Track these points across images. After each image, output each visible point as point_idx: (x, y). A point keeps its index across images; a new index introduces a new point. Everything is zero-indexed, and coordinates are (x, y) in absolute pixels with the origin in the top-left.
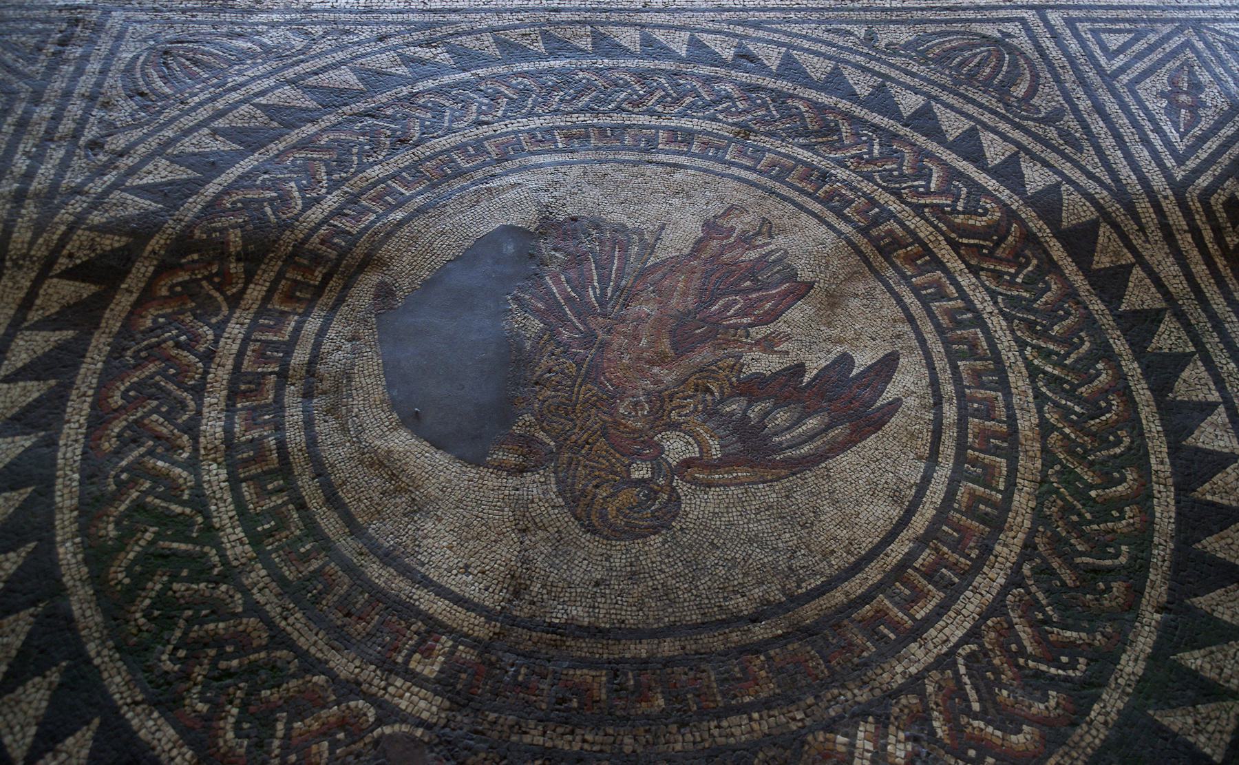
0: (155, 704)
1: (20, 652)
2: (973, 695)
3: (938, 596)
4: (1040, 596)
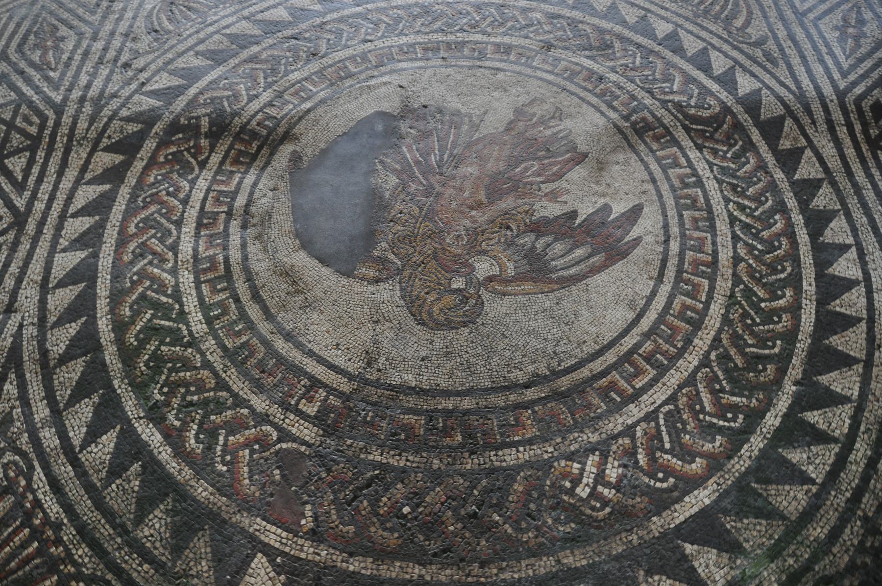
0: (151, 420)
1: (77, 383)
3: (653, 372)
4: (720, 373)
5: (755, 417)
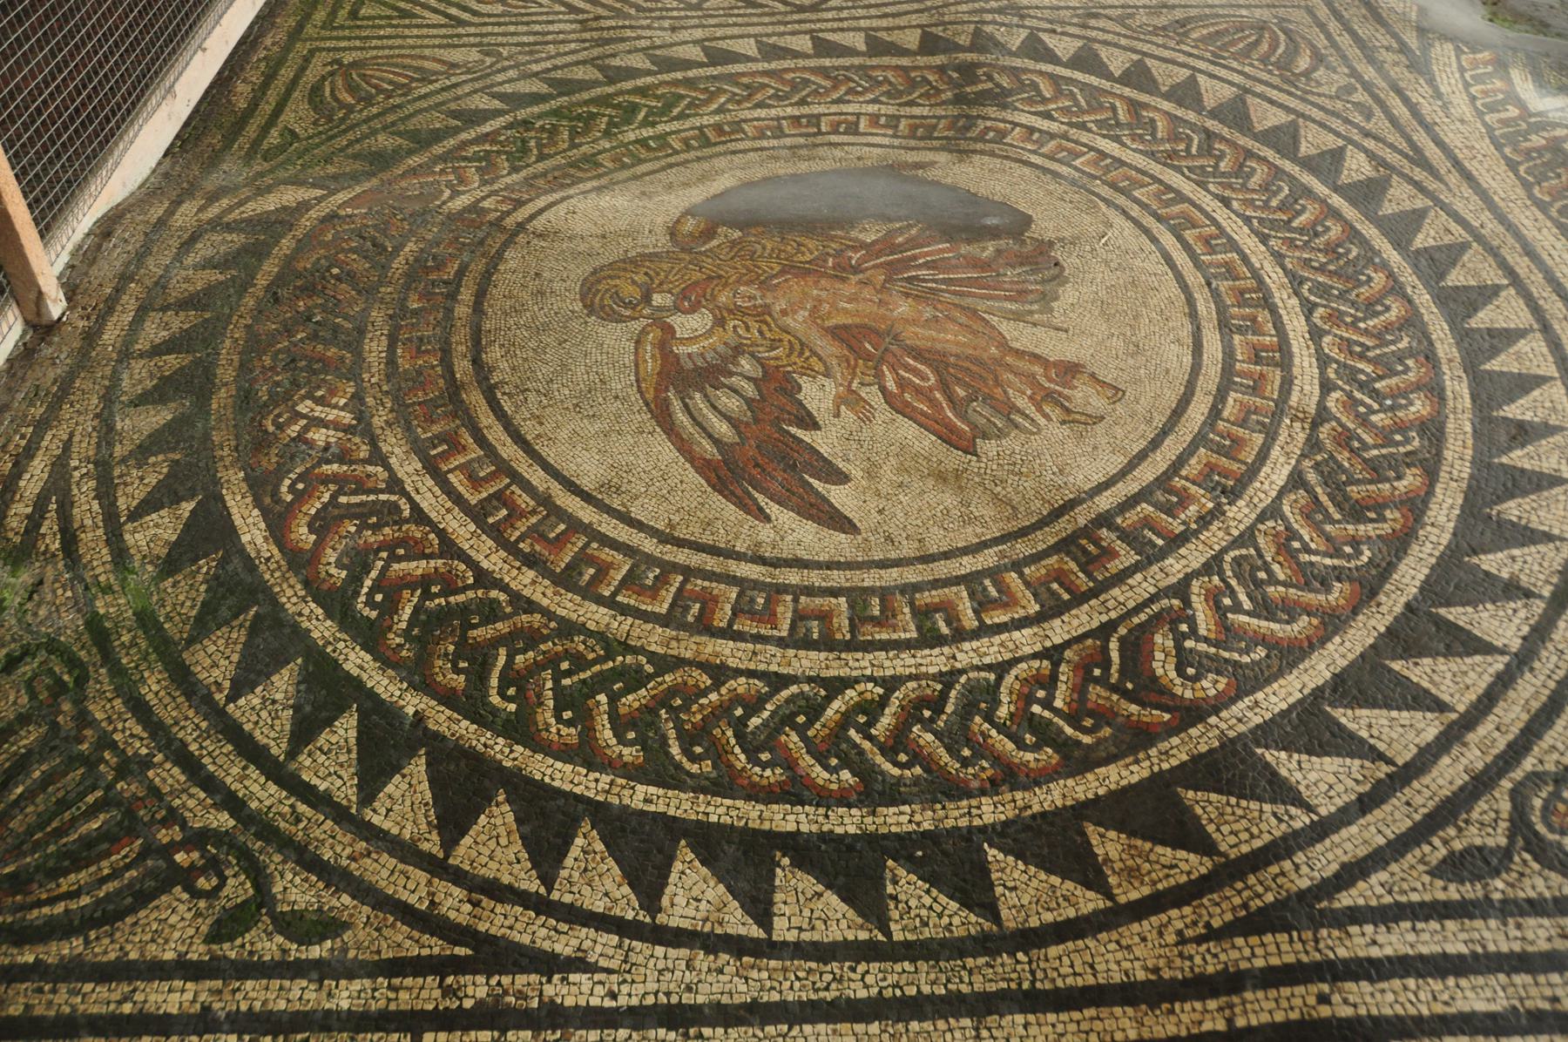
2: (355, 499)
4: (461, 598)
5: (370, 637)
